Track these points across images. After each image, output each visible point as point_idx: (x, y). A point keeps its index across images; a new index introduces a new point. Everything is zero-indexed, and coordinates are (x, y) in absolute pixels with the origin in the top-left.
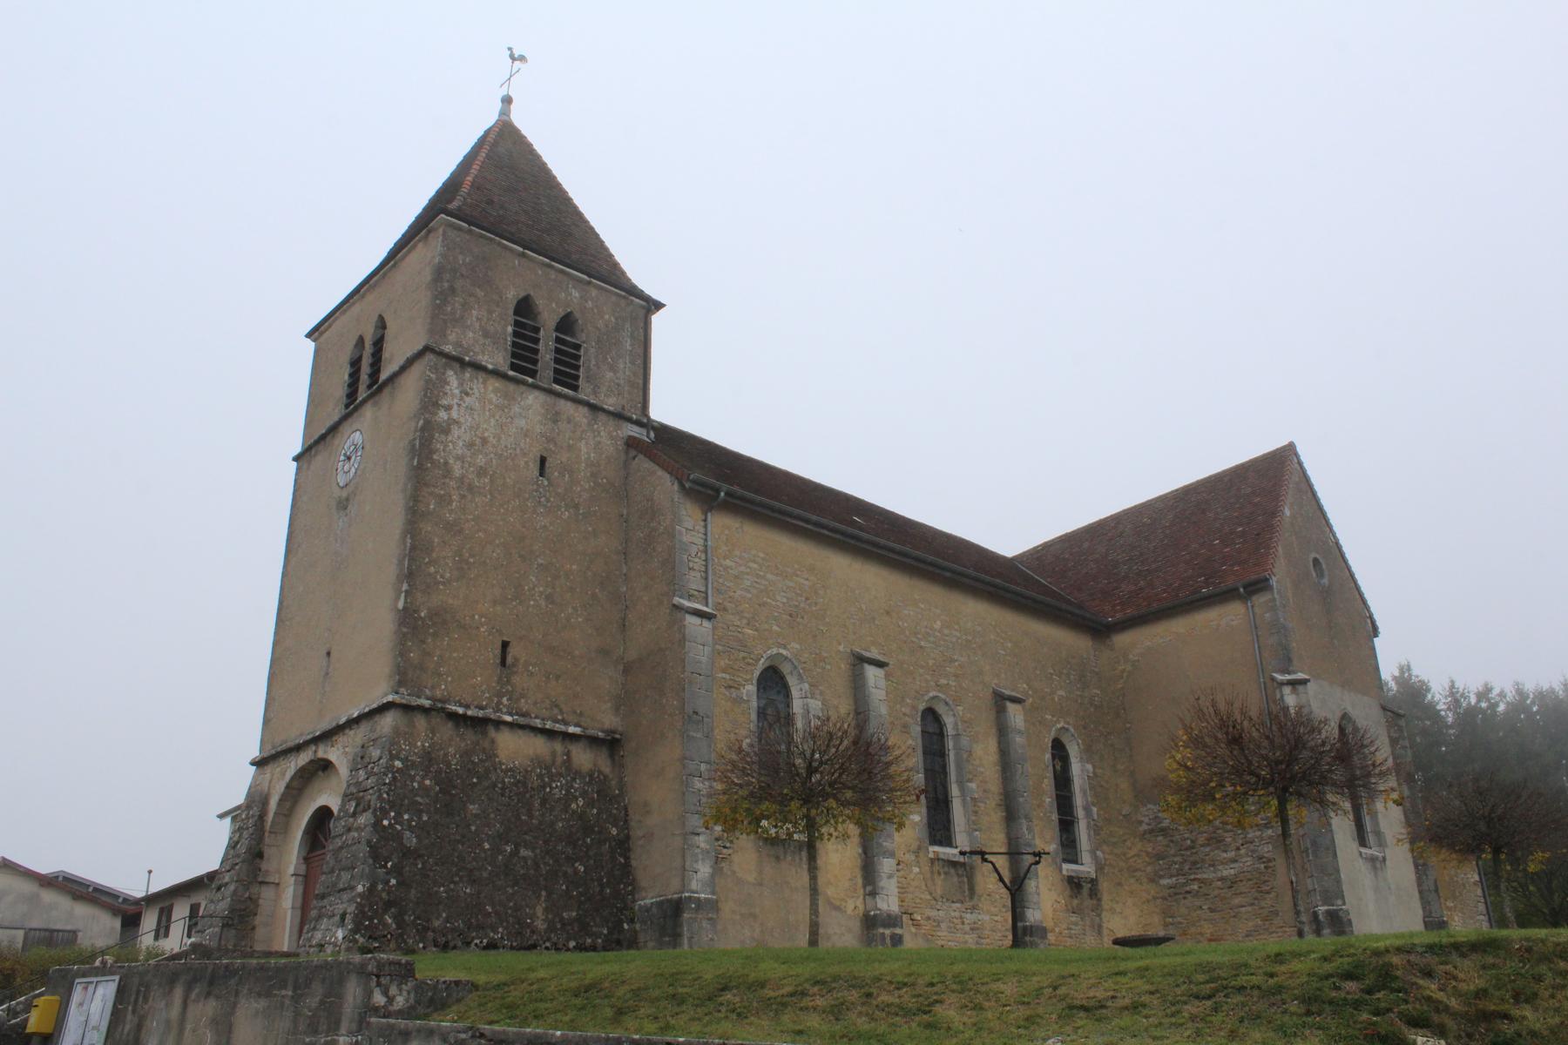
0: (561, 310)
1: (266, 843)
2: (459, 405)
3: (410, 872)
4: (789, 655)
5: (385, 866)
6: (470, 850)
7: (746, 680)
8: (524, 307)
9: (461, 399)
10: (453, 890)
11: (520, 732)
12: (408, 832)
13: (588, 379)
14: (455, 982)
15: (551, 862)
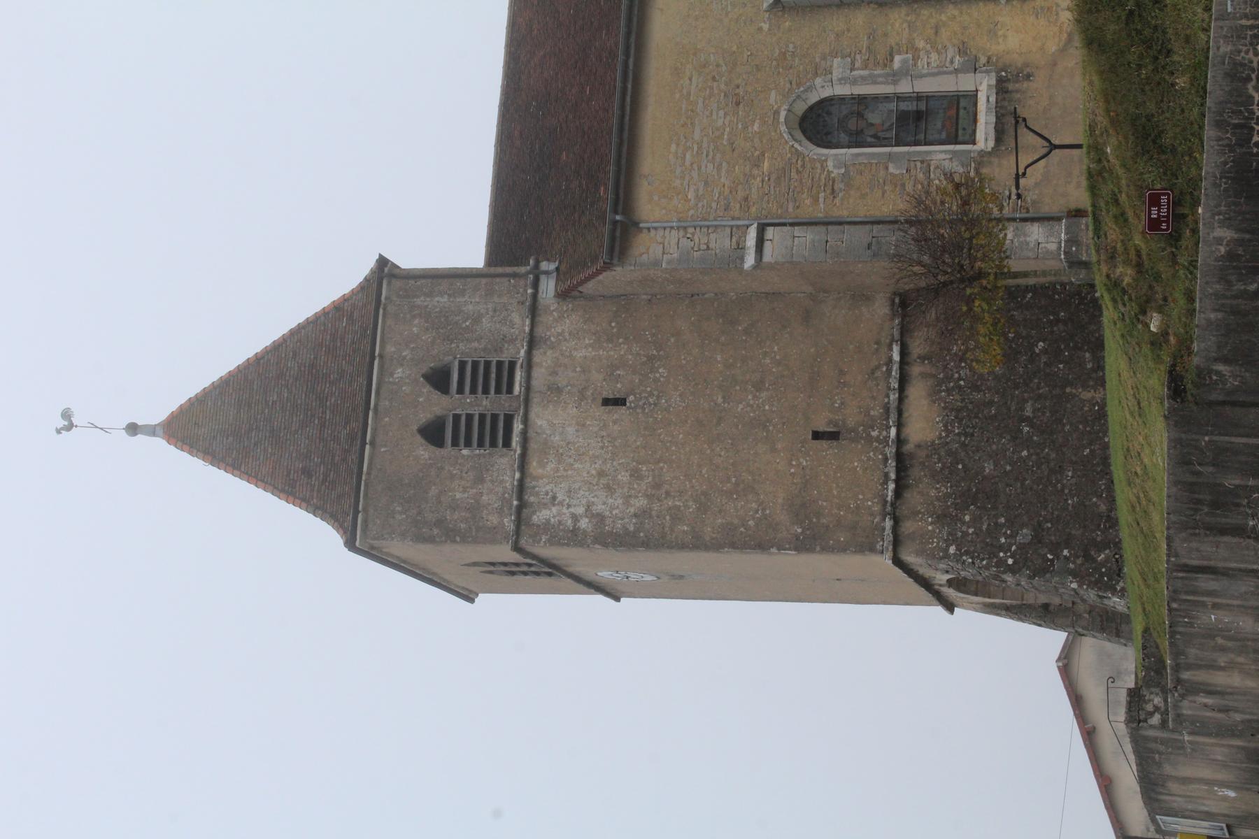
0: (425, 391)
1: (1034, 602)
2: (569, 506)
3: (1055, 535)
4: (786, 107)
5: (1052, 561)
6: (1030, 472)
7: (823, 168)
8: (433, 433)
9: (561, 503)
10: (1070, 490)
11: (905, 415)
12: (1018, 538)
13: (499, 350)
14: (1143, 650)
15: (1036, 381)
